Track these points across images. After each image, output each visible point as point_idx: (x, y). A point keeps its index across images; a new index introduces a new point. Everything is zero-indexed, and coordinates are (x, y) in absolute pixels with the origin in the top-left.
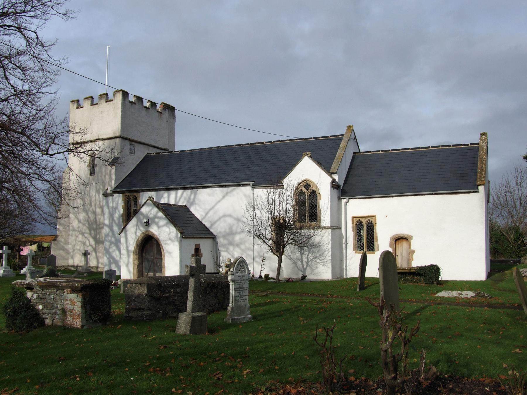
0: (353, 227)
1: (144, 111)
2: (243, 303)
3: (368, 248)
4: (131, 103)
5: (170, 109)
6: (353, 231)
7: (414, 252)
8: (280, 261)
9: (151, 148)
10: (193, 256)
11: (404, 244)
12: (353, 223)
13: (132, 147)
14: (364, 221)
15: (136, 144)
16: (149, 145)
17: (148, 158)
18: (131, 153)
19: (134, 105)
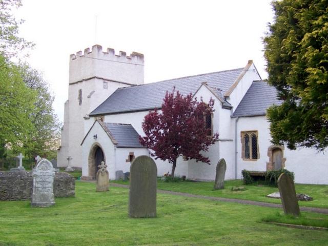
0: (241, 140)
1: (115, 59)
2: (46, 193)
3: (253, 157)
4: (105, 53)
5: (140, 56)
6: (242, 142)
7: (285, 159)
8: (174, 166)
9: (121, 84)
10: (127, 161)
11: (279, 152)
12: (241, 137)
13: (105, 84)
14: (250, 135)
15: (109, 82)
16: (120, 82)
17: (118, 92)
18: (104, 88)
19: (106, 55)
